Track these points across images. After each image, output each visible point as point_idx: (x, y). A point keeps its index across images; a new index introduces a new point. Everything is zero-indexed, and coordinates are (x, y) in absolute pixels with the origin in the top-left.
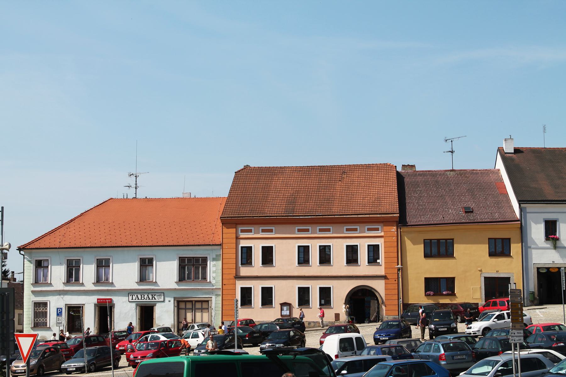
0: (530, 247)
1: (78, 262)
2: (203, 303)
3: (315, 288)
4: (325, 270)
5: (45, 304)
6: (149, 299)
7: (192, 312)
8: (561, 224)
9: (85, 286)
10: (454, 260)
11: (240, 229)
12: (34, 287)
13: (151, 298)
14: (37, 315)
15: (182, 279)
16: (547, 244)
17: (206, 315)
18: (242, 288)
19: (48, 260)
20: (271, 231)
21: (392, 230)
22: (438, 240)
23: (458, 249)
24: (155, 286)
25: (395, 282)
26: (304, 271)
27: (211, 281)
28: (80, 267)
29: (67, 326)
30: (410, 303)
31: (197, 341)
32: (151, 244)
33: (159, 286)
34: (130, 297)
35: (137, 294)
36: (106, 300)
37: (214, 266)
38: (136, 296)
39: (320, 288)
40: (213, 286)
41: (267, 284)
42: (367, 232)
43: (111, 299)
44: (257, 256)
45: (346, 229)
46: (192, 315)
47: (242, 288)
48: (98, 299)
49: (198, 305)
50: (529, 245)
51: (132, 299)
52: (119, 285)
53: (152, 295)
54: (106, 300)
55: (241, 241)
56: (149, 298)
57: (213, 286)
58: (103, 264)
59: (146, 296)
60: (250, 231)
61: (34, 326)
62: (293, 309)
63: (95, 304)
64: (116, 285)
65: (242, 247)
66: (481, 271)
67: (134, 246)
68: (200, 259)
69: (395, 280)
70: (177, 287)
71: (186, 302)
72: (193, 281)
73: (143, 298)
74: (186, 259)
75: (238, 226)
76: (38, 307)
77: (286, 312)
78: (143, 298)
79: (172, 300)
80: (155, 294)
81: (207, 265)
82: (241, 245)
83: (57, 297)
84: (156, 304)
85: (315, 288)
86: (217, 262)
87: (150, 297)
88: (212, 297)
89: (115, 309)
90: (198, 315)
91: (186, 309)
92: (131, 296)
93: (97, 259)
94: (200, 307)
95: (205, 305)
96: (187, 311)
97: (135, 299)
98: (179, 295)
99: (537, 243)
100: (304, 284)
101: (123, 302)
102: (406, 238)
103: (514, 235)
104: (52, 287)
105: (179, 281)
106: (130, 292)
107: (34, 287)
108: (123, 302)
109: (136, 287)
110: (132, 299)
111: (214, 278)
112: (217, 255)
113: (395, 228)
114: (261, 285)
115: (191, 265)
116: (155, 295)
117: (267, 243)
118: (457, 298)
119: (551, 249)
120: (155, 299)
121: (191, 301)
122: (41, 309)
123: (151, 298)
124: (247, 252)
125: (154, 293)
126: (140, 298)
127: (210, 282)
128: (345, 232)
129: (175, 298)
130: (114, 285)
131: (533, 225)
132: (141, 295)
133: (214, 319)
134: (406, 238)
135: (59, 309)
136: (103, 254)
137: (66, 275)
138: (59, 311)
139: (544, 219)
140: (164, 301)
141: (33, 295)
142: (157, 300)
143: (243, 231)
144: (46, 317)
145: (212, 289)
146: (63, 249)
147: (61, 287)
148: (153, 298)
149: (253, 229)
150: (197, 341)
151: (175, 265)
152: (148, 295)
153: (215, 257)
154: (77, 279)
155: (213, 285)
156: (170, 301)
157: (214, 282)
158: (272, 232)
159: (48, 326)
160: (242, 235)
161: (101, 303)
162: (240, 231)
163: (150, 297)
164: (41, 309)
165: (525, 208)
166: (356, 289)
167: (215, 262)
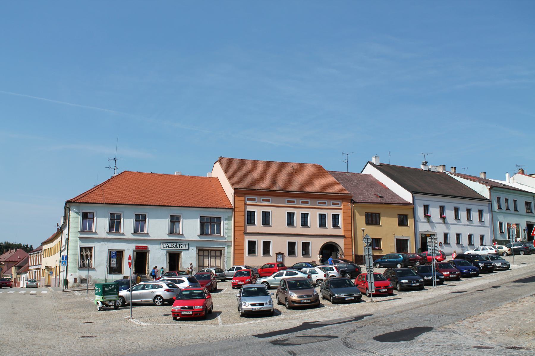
0: (417, 221)
1: (119, 217)
2: (204, 251)
3: (299, 243)
4: (305, 231)
5: (90, 249)
6: (177, 247)
7: (209, 258)
8: (431, 208)
9: (98, 234)
10: (381, 227)
11: (247, 198)
12: (81, 235)
13: (178, 247)
14: (82, 257)
15: (202, 233)
16: (425, 219)
17: (218, 261)
18: (249, 241)
19: (94, 213)
20: (269, 201)
21: (348, 205)
22: (372, 213)
23: (383, 220)
24: (182, 238)
25: (350, 240)
26: (291, 230)
27: (224, 235)
28: (120, 220)
29: (109, 267)
30: (358, 254)
31: (317, 276)
32: (180, 205)
33: (185, 238)
34: (162, 246)
35: (168, 243)
36: (143, 247)
37: (227, 224)
38: (167, 244)
39: (303, 243)
40: (226, 239)
41: (267, 239)
42: (301, 204)
43: (147, 246)
44: (258, 218)
45: (287, 201)
46: (208, 261)
47: (249, 241)
48: (136, 246)
49: (213, 253)
50: (417, 220)
51: (164, 247)
52: (152, 236)
53: (180, 245)
54: (143, 247)
55: (248, 207)
56: (177, 246)
57: (226, 239)
58: (140, 219)
59: (174, 245)
60: (254, 200)
61: (80, 267)
62: (285, 257)
63: (133, 250)
64: (150, 236)
65: (248, 211)
66: (394, 234)
67: (174, 206)
68: (216, 218)
69: (350, 239)
70: (199, 239)
71: (204, 250)
72: (210, 235)
73: (172, 247)
74: (216, 218)
75: (247, 195)
76: (84, 251)
77: (280, 260)
78: (172, 247)
79: (195, 249)
80: (182, 244)
81: (221, 223)
82: (248, 210)
83: (101, 243)
84: (182, 252)
85: (299, 243)
86: (229, 221)
87: (170, 245)
88: (224, 248)
89: (149, 254)
90: (213, 261)
91: (203, 256)
92: (163, 244)
93: (135, 215)
94: (215, 255)
95: (218, 254)
96: (204, 257)
97: (166, 247)
98: (200, 245)
99: (421, 219)
100: (292, 240)
101: (156, 249)
102: (356, 211)
103: (409, 213)
104: (97, 235)
105: (200, 234)
106: (162, 242)
107: (81, 234)
108: (156, 249)
109: (167, 237)
110: (164, 247)
111: (227, 233)
112: (228, 217)
113: (350, 203)
114: (262, 239)
115: (209, 223)
116: (182, 245)
117: (266, 209)
118: (383, 252)
119: (426, 223)
120: (182, 248)
121: (208, 250)
122: (86, 253)
123: (178, 247)
124: (251, 214)
125: (181, 243)
126: (170, 246)
127: (223, 236)
128: (331, 205)
129: (197, 248)
130: (184, 236)
131: (418, 207)
132: (171, 244)
133: (226, 264)
134: (356, 211)
135: (113, 253)
136: (140, 211)
137: (109, 226)
138: (113, 254)
139: (423, 204)
140: (188, 249)
141: (80, 241)
142: (183, 248)
143: (249, 199)
144: (91, 259)
145: (226, 241)
146: (141, 206)
147: (105, 235)
148: (180, 247)
149: (256, 198)
150: (317, 276)
151: (197, 222)
152: (176, 245)
153: (227, 217)
154: (118, 229)
155: (225, 239)
156: (193, 250)
157: (226, 236)
158: (308, 203)
159: (93, 267)
160: (249, 203)
161: (138, 250)
162: (247, 199)
163: (170, 245)
164: (86, 253)
165: (415, 196)
166: (327, 244)
167: (227, 222)
